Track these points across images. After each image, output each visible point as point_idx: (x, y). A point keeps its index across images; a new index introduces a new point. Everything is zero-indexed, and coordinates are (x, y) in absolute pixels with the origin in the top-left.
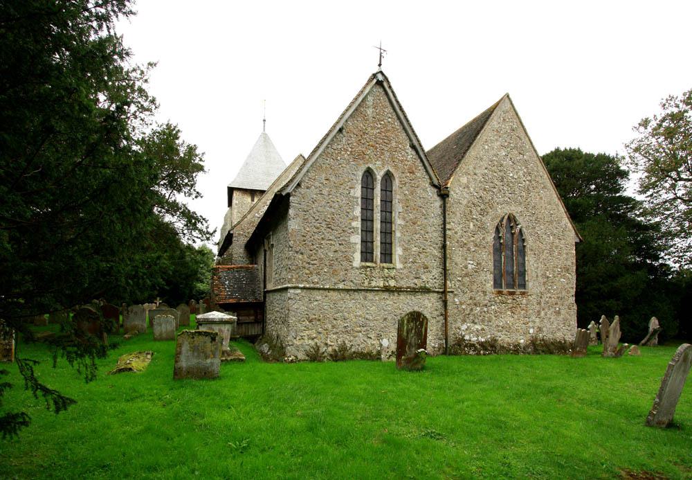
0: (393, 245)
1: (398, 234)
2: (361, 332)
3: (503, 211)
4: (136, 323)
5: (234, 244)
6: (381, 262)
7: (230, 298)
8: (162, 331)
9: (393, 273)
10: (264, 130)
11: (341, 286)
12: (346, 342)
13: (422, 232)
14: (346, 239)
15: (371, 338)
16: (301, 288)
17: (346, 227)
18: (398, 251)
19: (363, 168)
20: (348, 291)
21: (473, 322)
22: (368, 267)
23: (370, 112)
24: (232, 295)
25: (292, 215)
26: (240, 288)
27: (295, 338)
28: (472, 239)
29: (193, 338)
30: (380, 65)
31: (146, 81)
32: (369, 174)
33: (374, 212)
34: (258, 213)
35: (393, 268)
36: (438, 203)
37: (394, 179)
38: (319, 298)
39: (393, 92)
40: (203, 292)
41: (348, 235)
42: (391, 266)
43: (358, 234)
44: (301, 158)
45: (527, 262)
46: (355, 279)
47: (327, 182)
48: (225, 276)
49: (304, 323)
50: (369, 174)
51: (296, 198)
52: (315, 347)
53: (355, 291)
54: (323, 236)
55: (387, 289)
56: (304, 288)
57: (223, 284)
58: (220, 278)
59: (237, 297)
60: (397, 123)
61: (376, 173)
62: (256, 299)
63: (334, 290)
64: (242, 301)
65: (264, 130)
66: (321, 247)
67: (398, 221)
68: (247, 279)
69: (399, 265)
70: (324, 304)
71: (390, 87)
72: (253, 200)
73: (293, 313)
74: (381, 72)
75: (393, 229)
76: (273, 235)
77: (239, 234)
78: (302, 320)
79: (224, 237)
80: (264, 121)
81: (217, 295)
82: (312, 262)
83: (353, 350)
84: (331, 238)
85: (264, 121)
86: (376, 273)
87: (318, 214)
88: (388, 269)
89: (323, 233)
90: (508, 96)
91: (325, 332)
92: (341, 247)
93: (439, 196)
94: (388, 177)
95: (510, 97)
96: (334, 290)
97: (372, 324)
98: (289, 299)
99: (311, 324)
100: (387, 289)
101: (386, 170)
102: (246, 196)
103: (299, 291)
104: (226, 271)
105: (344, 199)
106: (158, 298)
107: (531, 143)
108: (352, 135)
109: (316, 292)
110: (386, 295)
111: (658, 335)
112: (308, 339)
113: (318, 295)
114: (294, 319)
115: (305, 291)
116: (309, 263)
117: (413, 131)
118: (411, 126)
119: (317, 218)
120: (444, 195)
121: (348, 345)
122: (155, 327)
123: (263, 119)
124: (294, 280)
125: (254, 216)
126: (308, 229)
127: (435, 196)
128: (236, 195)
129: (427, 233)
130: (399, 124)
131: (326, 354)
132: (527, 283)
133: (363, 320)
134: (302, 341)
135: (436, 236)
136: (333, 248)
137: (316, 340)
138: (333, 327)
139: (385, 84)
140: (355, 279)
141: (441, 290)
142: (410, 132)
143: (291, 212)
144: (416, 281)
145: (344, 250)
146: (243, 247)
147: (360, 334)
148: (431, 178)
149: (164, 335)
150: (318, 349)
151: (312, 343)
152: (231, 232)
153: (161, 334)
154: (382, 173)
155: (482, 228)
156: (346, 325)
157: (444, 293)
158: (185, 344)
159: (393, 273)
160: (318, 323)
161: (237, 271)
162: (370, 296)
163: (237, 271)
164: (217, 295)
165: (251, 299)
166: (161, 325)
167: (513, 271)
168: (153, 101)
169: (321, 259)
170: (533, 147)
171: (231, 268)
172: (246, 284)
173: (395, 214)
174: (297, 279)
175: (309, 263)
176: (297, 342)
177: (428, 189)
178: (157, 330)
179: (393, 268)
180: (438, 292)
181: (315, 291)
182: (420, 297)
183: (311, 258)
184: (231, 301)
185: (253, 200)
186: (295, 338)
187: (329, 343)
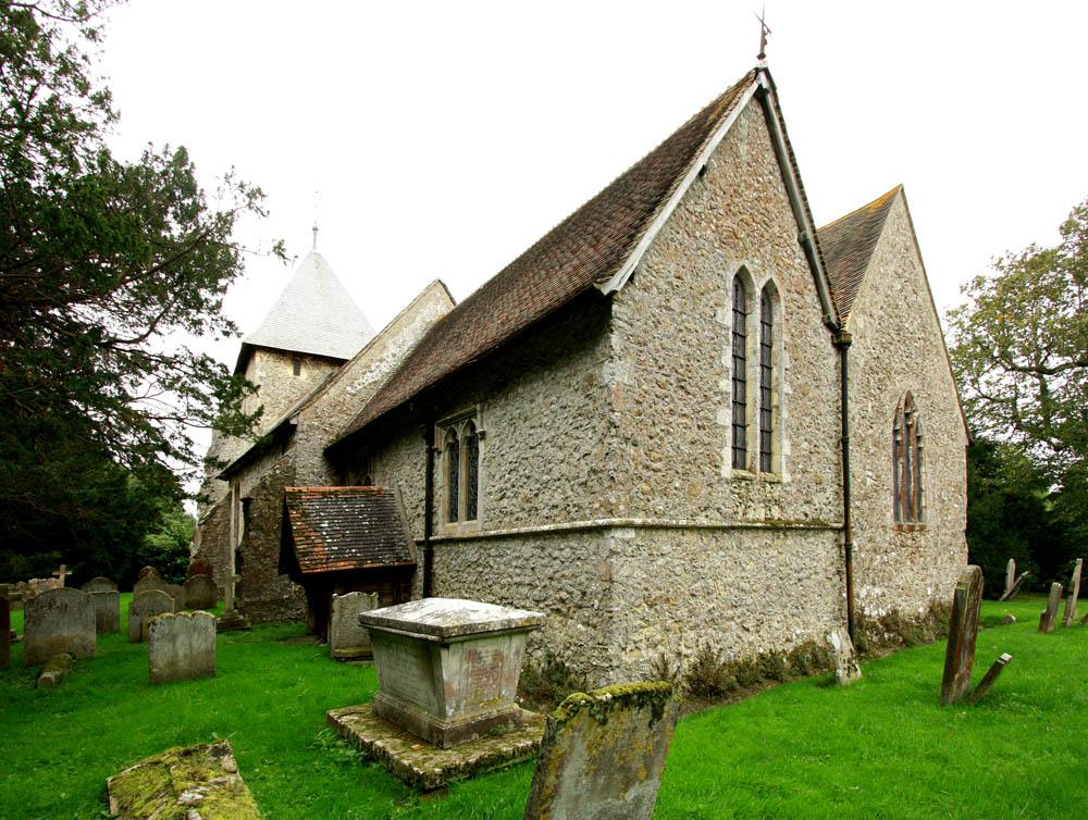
0: (774, 435)
1: (785, 414)
2: (733, 618)
3: (902, 384)
4: (65, 634)
5: (298, 447)
6: (762, 470)
7: (338, 560)
8: (176, 655)
9: (777, 491)
10: (314, 248)
11: (702, 521)
12: (712, 644)
13: (814, 413)
14: (711, 417)
15: (748, 630)
16: (637, 528)
17: (710, 389)
18: (783, 448)
19: (734, 267)
20: (713, 529)
21: (874, 584)
22: (744, 479)
23: (743, 149)
24: (341, 551)
25: (617, 348)
26: (358, 536)
27: (624, 649)
28: (871, 431)
29: (604, 722)
30: (761, 56)
31: (92, 35)
32: (742, 278)
33: (748, 363)
34: (351, 385)
35: (779, 482)
36: (833, 360)
37: (778, 301)
38: (666, 548)
39: (781, 120)
40: (160, 551)
41: (713, 407)
42: (769, 477)
43: (728, 407)
44: (439, 291)
45: (924, 477)
46: (724, 504)
47: (679, 282)
48: (318, 511)
49: (639, 610)
50: (742, 278)
51: (624, 309)
52: (659, 663)
53: (724, 529)
54: (671, 406)
55: (773, 527)
56: (644, 527)
57: (317, 528)
58: (305, 514)
59: (354, 557)
60: (781, 188)
61: (756, 284)
62: (399, 559)
63: (691, 529)
64: (369, 564)
65: (314, 248)
66: (669, 433)
67: (784, 389)
68: (370, 515)
69: (786, 478)
70: (677, 562)
71: (778, 108)
72: (297, 373)
73: (620, 589)
74: (766, 71)
75: (775, 403)
76: (482, 411)
77: (311, 427)
78: (637, 603)
79: (368, 419)
80: (315, 229)
81: (305, 554)
82: (655, 465)
83: (722, 660)
84: (686, 411)
85: (315, 229)
86: (755, 492)
87: (662, 353)
88: (770, 483)
89: (673, 400)
90: (903, 190)
91: (676, 625)
92: (702, 432)
93: (834, 345)
94: (769, 292)
95: (905, 191)
96: (691, 529)
97: (750, 601)
98: (613, 553)
99: (653, 611)
100: (773, 527)
101: (767, 278)
102: (282, 364)
103: (631, 534)
104: (319, 500)
105: (706, 327)
106: (63, 567)
107: (926, 278)
108: (718, 191)
109: (662, 536)
110: (767, 538)
111: (1003, 587)
112: (648, 647)
113: (664, 542)
114: (623, 602)
115: (642, 533)
116: (647, 467)
117: (808, 210)
118: (805, 199)
119: (661, 363)
120: (842, 346)
121: (715, 651)
122: (156, 645)
123: (313, 225)
124: (622, 507)
125: (344, 392)
126: (645, 387)
127: (830, 346)
128: (259, 360)
129: (820, 415)
130: (784, 190)
131: (679, 676)
132: (924, 510)
133: (736, 592)
134: (636, 653)
135: (830, 421)
136: (690, 436)
137: (661, 648)
138: (691, 613)
139: (770, 98)
140: (724, 504)
141: (841, 525)
142: (803, 210)
143: (615, 339)
144: (806, 508)
145: (707, 440)
146: (320, 453)
147: (733, 623)
148: (824, 310)
149: (183, 665)
150: (666, 669)
151: (654, 655)
152: (293, 422)
153: (172, 663)
154: (762, 284)
155: (880, 413)
156: (711, 606)
157: (846, 529)
158: (575, 754)
159: (777, 491)
160: (666, 607)
161: (346, 499)
162: (747, 538)
163: (346, 499)
164: (305, 554)
165: (387, 560)
166: (173, 638)
167: (909, 490)
168: (101, 100)
169: (669, 459)
170: (928, 284)
171: (330, 493)
172: (370, 527)
173: (780, 372)
174: (627, 505)
175: (647, 467)
176: (627, 658)
177: (820, 331)
178: (162, 653)
179: (779, 482)
180: (833, 529)
181: (661, 532)
182: (812, 539)
183: (653, 454)
184: (342, 566)
185: (297, 373)
186: (624, 649)
187: (685, 651)
